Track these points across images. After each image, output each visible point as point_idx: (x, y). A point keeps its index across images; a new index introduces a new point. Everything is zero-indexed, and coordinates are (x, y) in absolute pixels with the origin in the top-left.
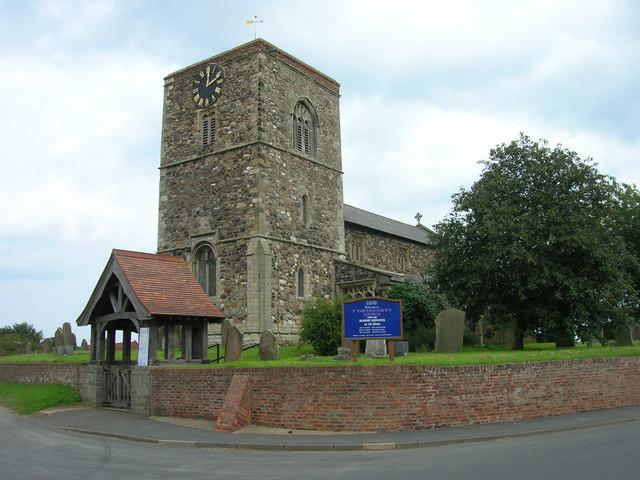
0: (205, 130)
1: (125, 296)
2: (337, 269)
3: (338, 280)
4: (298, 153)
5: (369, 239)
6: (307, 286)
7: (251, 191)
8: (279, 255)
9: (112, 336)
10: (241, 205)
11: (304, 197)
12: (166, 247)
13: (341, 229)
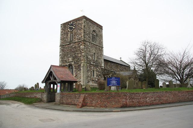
0: (71, 38)
1: (54, 76)
2: (102, 70)
3: (102, 73)
4: (93, 43)
5: (109, 63)
6: (95, 74)
7: (82, 52)
8: (89, 67)
9: (50, 86)
10: (79, 55)
11: (94, 53)
12: (61, 65)
13: (103, 61)
